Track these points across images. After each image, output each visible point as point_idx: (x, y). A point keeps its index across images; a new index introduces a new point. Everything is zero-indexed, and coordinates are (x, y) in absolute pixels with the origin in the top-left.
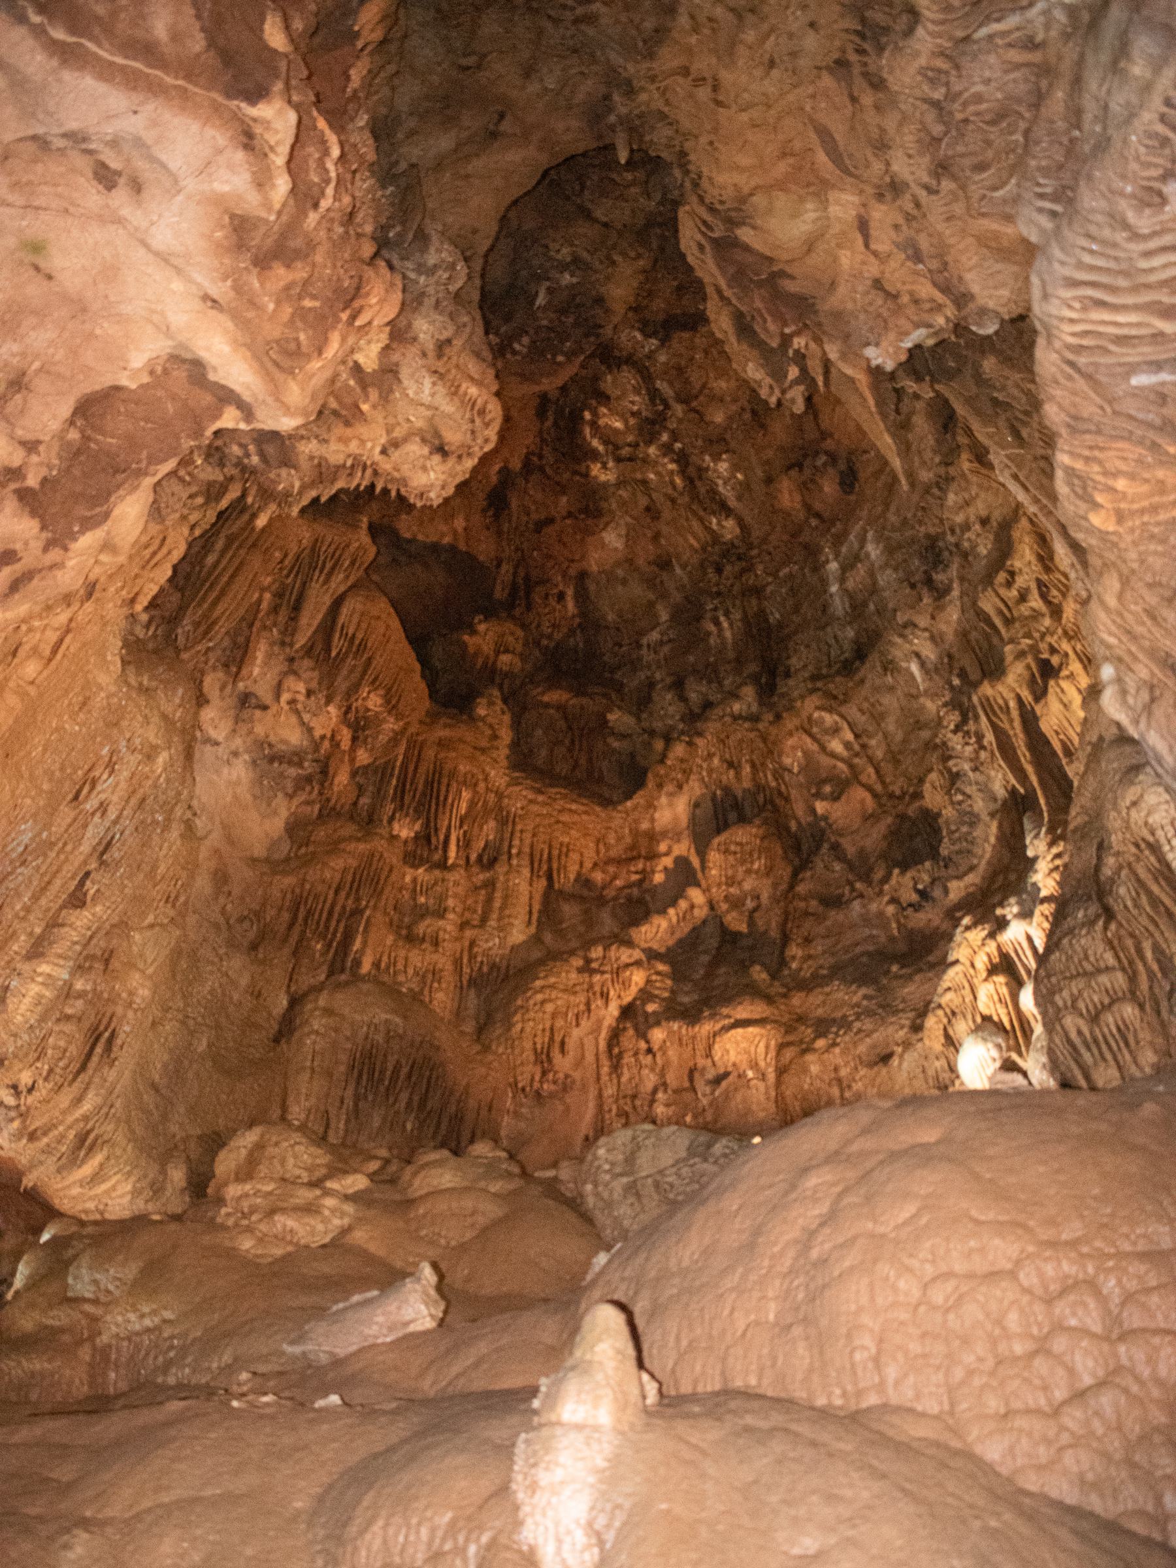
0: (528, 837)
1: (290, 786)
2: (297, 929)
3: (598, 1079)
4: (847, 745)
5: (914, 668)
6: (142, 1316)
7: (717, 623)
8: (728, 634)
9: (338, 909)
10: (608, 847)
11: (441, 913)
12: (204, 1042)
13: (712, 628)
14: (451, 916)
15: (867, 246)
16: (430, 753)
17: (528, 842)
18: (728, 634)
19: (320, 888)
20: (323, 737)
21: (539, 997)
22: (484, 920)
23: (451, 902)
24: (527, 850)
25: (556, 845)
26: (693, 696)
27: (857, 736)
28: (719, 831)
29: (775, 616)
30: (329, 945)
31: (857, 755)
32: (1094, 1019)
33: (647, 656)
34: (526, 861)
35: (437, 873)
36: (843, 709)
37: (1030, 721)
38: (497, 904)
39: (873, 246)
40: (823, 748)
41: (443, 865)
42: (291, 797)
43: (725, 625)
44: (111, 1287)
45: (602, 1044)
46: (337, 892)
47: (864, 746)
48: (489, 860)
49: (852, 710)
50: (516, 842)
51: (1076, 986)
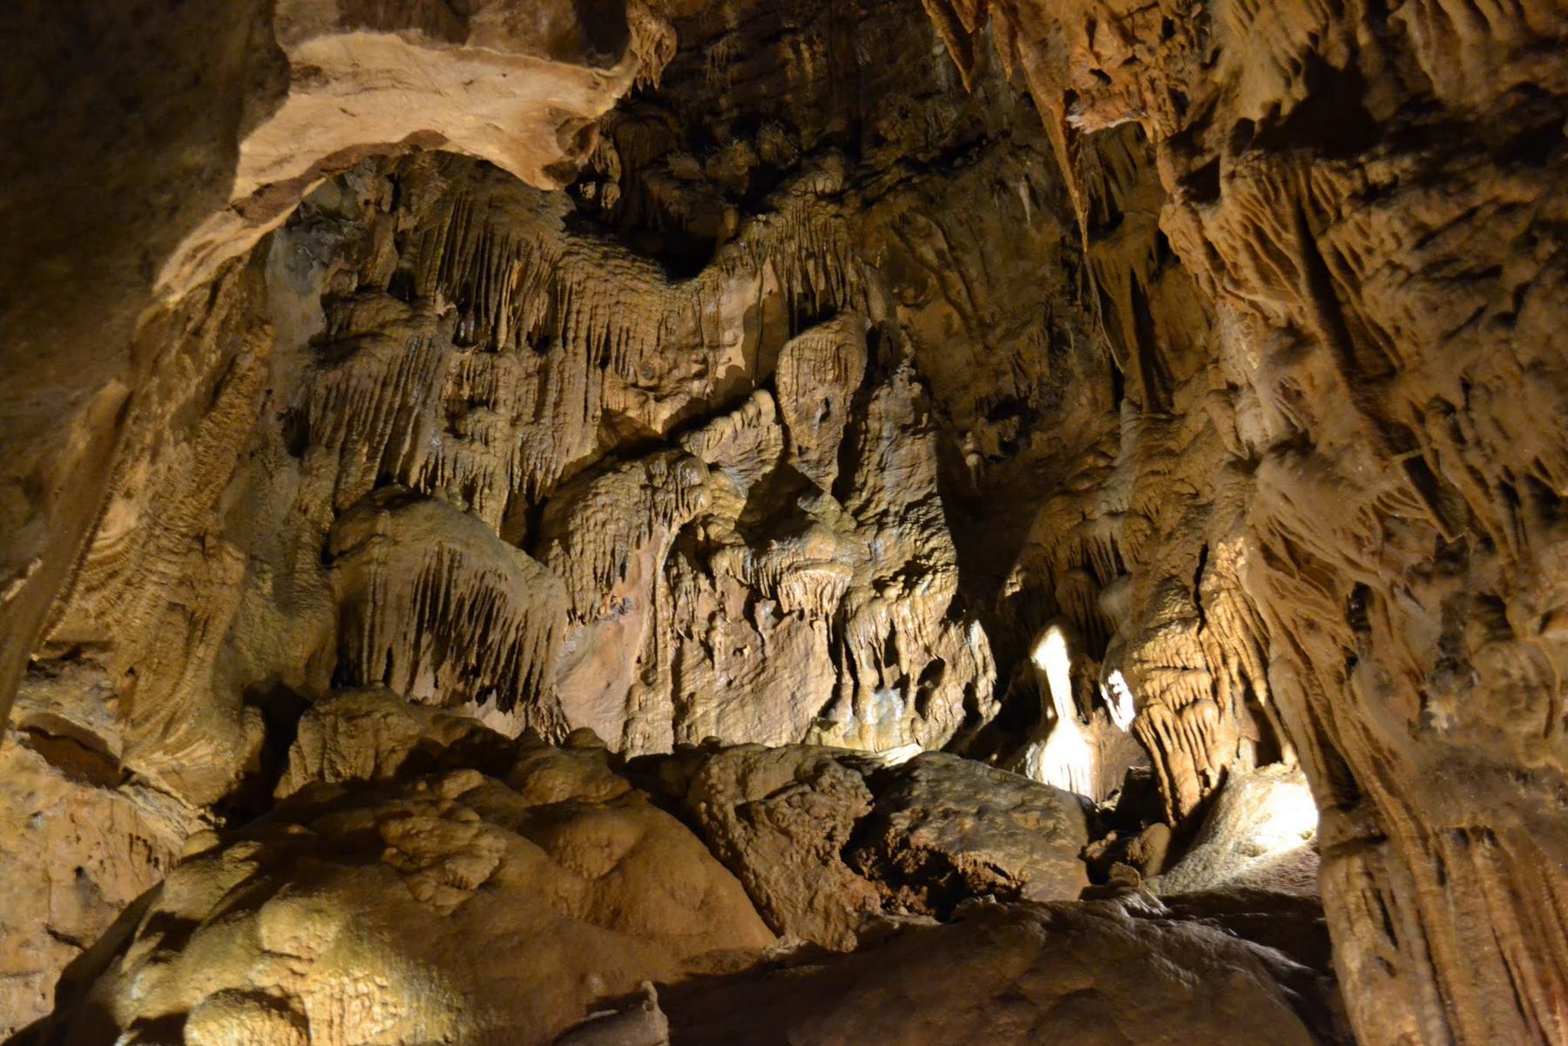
0: (585, 317)
1: (325, 253)
2: (342, 434)
3: (653, 602)
4: (940, 254)
5: (1023, 192)
6: (356, 980)
7: (797, 51)
8: (809, 67)
9: (385, 407)
10: (670, 332)
11: (489, 404)
12: (270, 583)
13: (790, 54)
14: (501, 410)
15: (1091, 45)
16: (480, 217)
17: (584, 326)
18: (809, 67)
19: (369, 384)
20: (367, 203)
21: (601, 516)
22: (538, 415)
23: (502, 394)
24: (583, 334)
25: (615, 331)
26: (767, 147)
27: (951, 248)
28: (792, 336)
29: (864, 58)
30: (376, 450)
31: (948, 266)
32: (1179, 712)
33: (712, 73)
34: (582, 350)
35: (486, 357)
36: (939, 216)
37: (1140, 302)
38: (552, 397)
39: (1096, 48)
40: (912, 250)
41: (492, 349)
42: (325, 266)
43: (806, 55)
44: (312, 945)
45: (661, 564)
46: (384, 385)
47: (957, 261)
48: (542, 342)
49: (948, 218)
50: (572, 324)
51: (1168, 677)
